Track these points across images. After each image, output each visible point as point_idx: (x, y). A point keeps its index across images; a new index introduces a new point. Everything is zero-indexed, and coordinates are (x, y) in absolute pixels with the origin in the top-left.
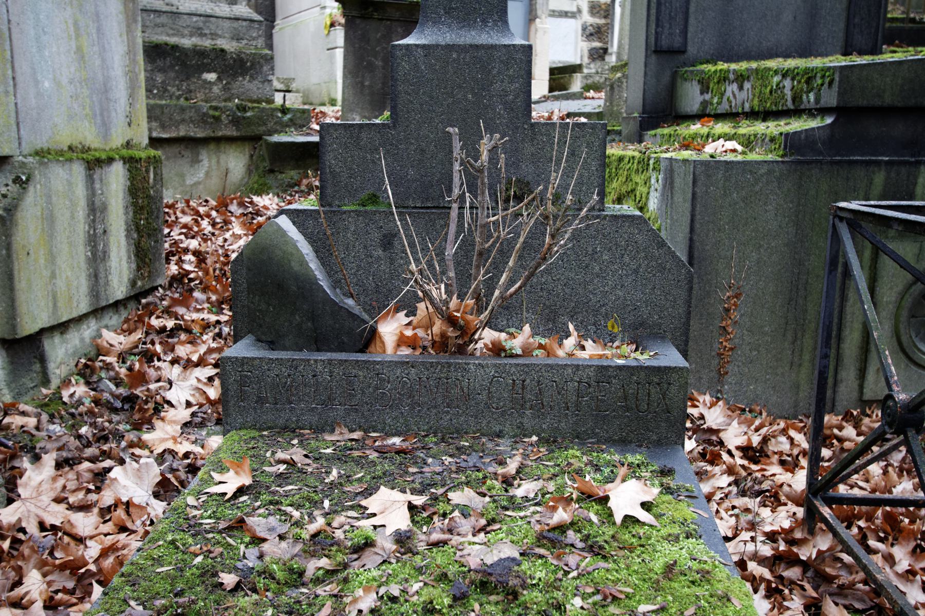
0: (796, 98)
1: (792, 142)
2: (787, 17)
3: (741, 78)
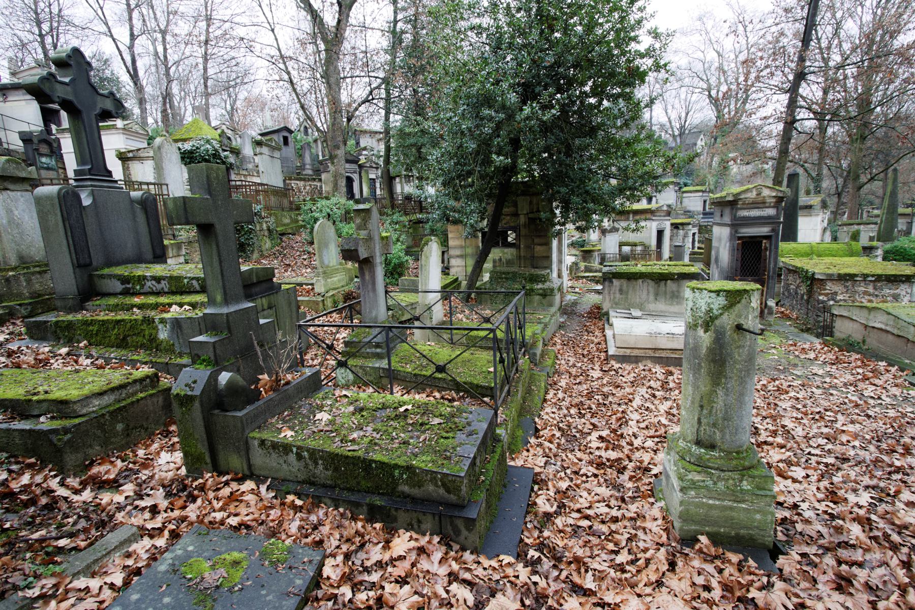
2: (129, 245)
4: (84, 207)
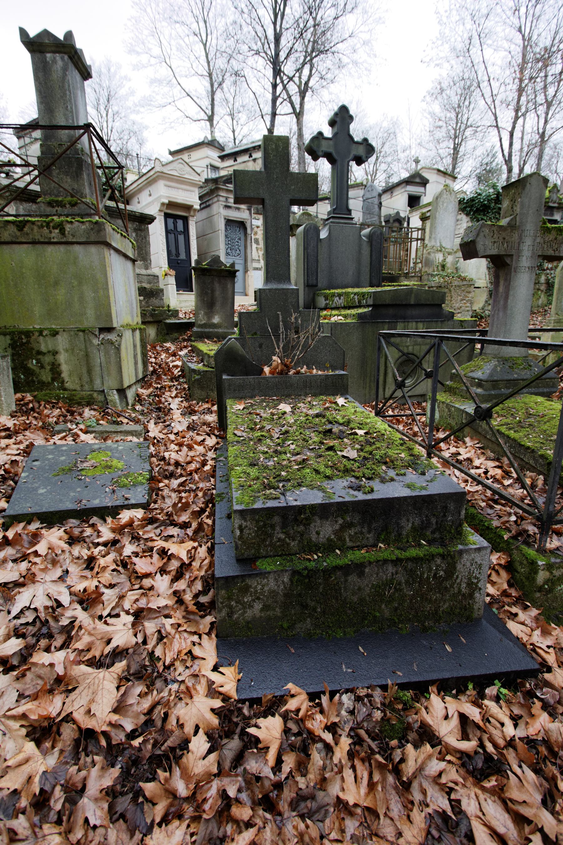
0: (359, 302)
1: (360, 316)
2: (351, 273)
3: (339, 295)
4: (321, 240)
